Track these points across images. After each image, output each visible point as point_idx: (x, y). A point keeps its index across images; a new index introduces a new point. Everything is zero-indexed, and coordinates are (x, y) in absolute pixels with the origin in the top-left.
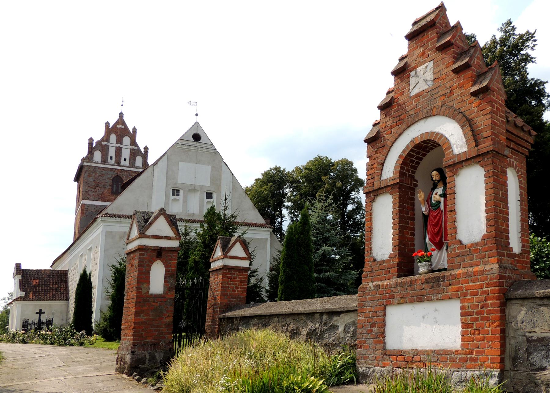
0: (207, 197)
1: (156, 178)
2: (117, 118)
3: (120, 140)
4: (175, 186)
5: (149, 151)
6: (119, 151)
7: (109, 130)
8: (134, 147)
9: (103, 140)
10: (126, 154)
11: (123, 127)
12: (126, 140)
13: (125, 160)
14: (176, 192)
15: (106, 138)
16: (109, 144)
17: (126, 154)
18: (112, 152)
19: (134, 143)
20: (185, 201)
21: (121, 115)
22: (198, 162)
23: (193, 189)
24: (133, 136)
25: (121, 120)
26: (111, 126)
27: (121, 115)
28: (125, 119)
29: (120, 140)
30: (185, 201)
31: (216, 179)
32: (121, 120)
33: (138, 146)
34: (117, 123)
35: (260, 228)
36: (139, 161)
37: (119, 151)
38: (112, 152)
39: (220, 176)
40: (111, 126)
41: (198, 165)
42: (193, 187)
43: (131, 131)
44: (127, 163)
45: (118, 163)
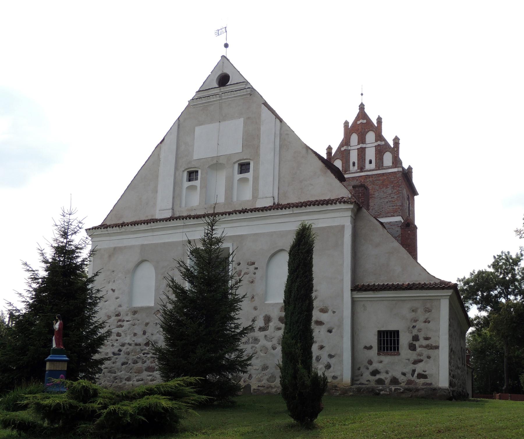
0: (241, 172)
1: (162, 160)
2: (358, 111)
3: (362, 140)
4: (190, 166)
5: (400, 142)
6: (362, 152)
7: (349, 131)
8: (379, 143)
9: (342, 145)
10: (370, 154)
11: (365, 121)
12: (370, 137)
13: (371, 162)
14: (192, 175)
15: (346, 142)
16: (349, 148)
17: (370, 154)
18: (354, 157)
19: (379, 137)
20: (205, 186)
21: (362, 107)
22: (223, 118)
23: (216, 165)
24: (378, 130)
25: (362, 114)
26: (350, 125)
27: (362, 107)
28: (366, 110)
29: (362, 140)
30: (205, 186)
31: (251, 140)
32: (362, 114)
33: (384, 140)
34: (358, 118)
35: (325, 208)
36: (388, 159)
37: (362, 152)
38: (354, 157)
39: (259, 129)
40: (350, 125)
41: (223, 124)
42: (215, 162)
43: (375, 122)
44: (373, 166)
45: (362, 168)
